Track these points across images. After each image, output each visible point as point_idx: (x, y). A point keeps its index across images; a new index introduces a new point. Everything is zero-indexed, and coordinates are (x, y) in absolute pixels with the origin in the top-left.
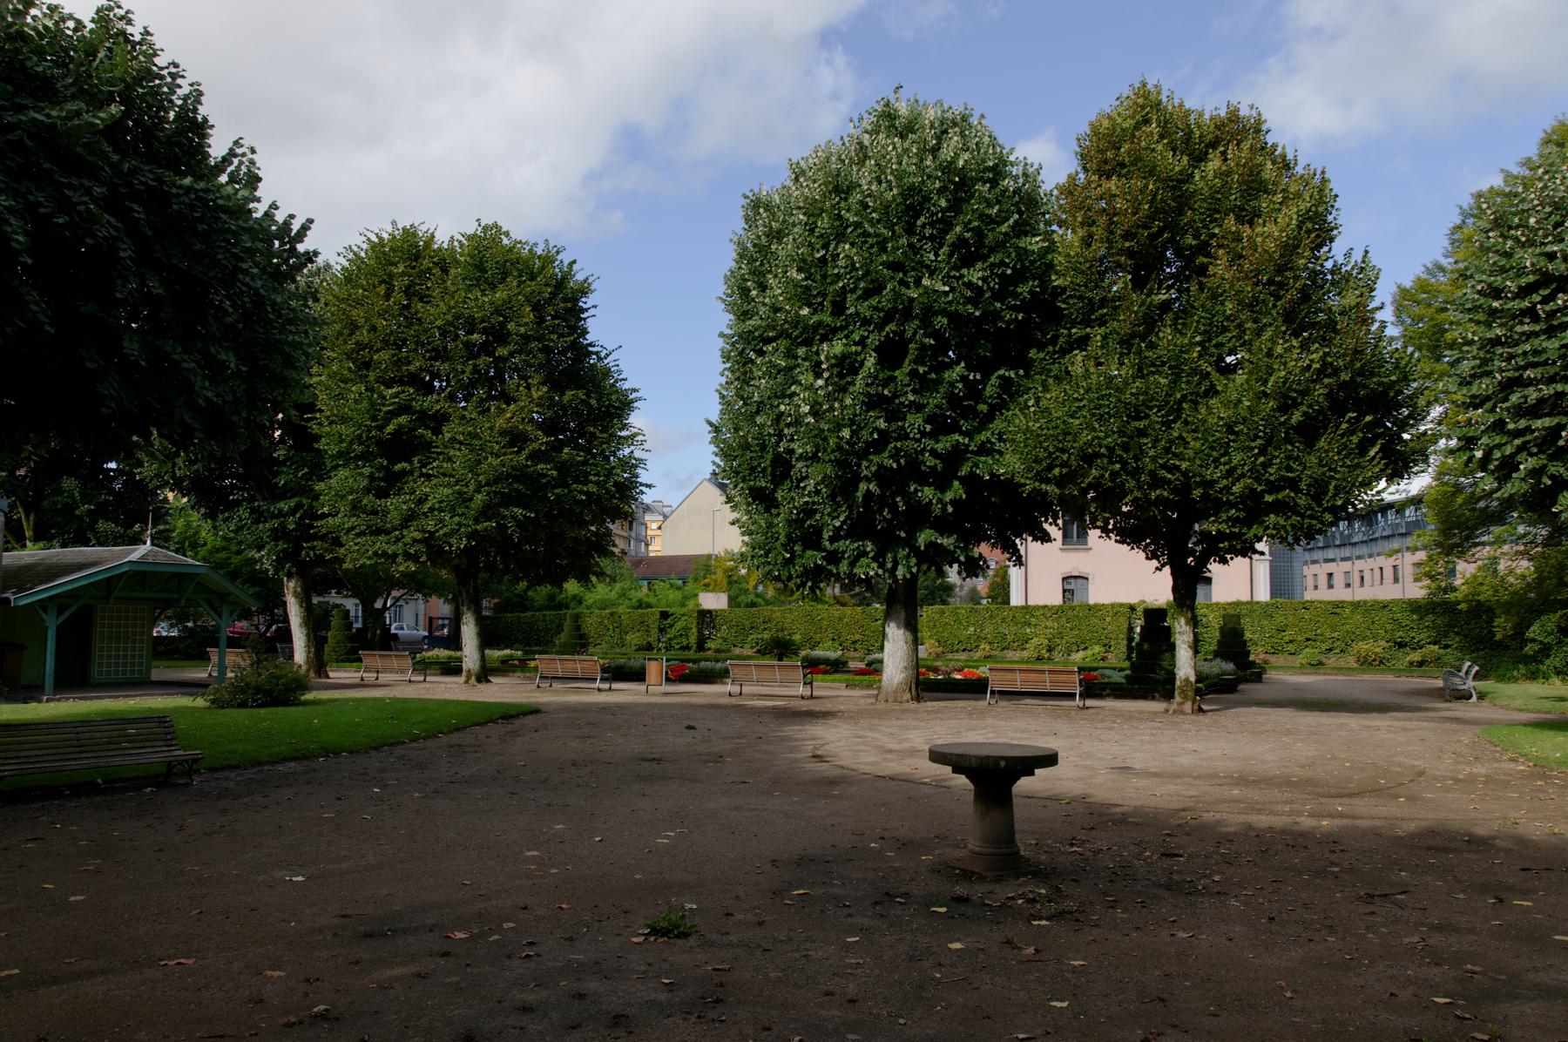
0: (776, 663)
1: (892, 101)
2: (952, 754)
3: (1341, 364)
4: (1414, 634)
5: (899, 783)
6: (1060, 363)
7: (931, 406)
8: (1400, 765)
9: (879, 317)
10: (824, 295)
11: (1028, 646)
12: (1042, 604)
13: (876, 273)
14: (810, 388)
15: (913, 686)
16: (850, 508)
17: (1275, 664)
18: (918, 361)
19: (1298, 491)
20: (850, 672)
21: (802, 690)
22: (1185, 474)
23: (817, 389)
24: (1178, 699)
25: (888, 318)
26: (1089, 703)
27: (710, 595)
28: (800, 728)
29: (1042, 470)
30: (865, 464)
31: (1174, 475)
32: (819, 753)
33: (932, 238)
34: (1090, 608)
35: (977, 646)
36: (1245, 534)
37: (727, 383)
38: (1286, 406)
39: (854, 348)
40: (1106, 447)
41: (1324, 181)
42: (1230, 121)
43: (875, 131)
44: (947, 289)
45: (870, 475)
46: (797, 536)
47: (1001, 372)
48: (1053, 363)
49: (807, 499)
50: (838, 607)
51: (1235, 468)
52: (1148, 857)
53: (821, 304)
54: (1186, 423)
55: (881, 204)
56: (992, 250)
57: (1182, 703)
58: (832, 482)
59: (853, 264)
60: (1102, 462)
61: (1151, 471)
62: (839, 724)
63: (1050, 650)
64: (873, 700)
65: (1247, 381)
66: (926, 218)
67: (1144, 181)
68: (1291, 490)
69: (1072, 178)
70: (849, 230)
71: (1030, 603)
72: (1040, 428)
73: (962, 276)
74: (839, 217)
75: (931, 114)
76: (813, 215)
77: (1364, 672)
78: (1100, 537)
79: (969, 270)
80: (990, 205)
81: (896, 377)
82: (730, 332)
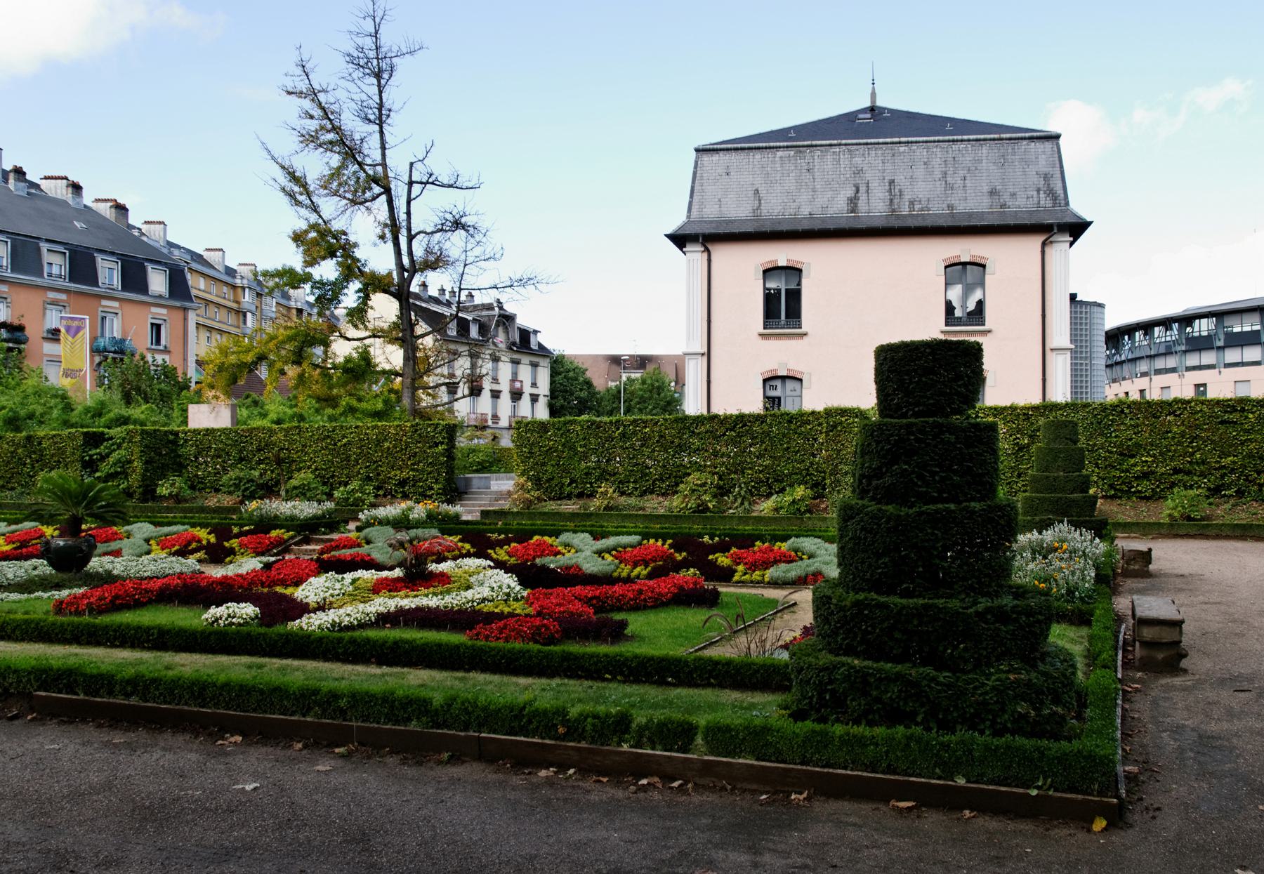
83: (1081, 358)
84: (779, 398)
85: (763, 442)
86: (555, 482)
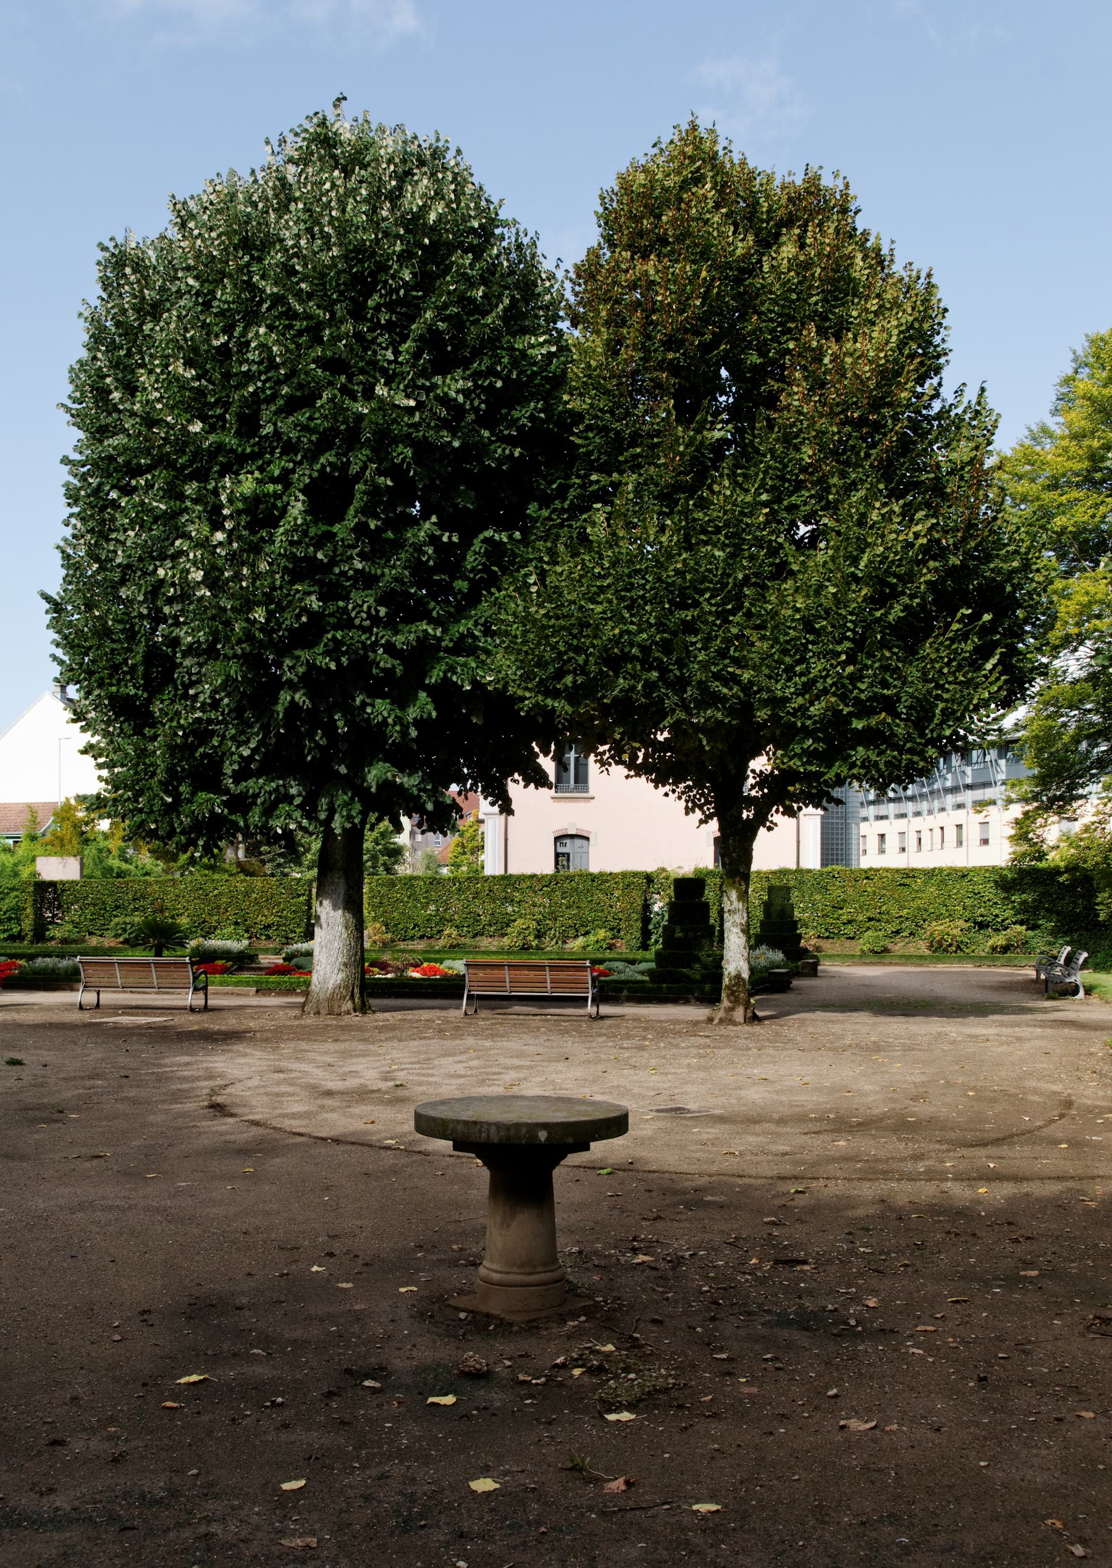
0: (151, 959)
1: (331, 118)
2: (458, 1121)
3: (951, 541)
4: (997, 911)
5: (349, 1147)
6: (570, 526)
7: (387, 578)
8: (1035, 1091)
9: (310, 441)
10: (226, 406)
11: (509, 930)
12: (529, 873)
13: (307, 373)
14: (204, 544)
15: (356, 990)
16: (265, 728)
17: (830, 952)
18: (368, 511)
19: (896, 715)
20: (261, 969)
21: (190, 998)
22: (747, 688)
23: (215, 547)
24: (726, 1003)
25: (324, 443)
26: (605, 1009)
27: (54, 860)
28: (186, 1059)
29: (548, 678)
30: (288, 662)
31: (731, 689)
32: (219, 1099)
33: (390, 326)
34: (593, 878)
35: (440, 932)
36: (824, 774)
37: (74, 536)
38: (883, 597)
39: (271, 487)
40: (639, 646)
41: (930, 287)
42: (807, 190)
43: (304, 160)
44: (412, 403)
45: (296, 679)
46: (183, 770)
47: (488, 533)
48: (561, 526)
49: (198, 714)
50: (242, 876)
51: (814, 681)
52: (757, 1267)
53: (221, 417)
54: (749, 615)
55: (314, 268)
56: (477, 353)
57: (732, 1009)
58: (237, 687)
59: (271, 358)
60: (634, 668)
61: (700, 682)
62: (248, 1051)
63: (539, 936)
64: (297, 1012)
65: (833, 559)
66: (381, 296)
67: (694, 267)
68: (888, 714)
69: (593, 254)
70: (265, 306)
71: (511, 871)
72: (546, 615)
73: (434, 386)
74: (250, 286)
75: (389, 145)
76: (207, 280)
77: (938, 960)
78: (627, 777)
79: (444, 378)
80: (472, 284)
81: (335, 534)
82: (77, 457)
83: (837, 818)
84: (568, 854)
85: (572, 896)
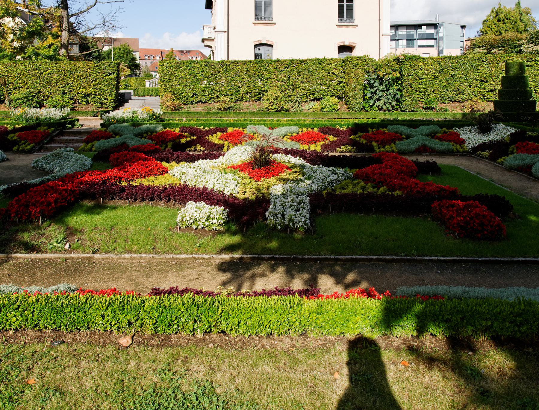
84: (261, 54)
86: (184, 95)
